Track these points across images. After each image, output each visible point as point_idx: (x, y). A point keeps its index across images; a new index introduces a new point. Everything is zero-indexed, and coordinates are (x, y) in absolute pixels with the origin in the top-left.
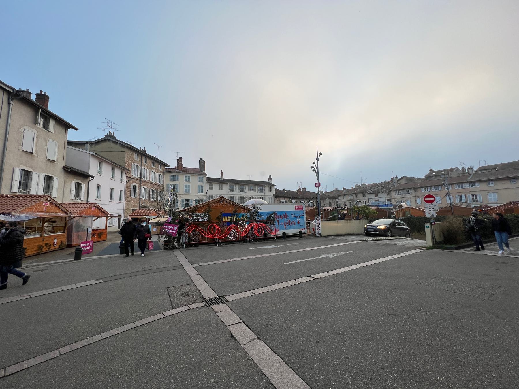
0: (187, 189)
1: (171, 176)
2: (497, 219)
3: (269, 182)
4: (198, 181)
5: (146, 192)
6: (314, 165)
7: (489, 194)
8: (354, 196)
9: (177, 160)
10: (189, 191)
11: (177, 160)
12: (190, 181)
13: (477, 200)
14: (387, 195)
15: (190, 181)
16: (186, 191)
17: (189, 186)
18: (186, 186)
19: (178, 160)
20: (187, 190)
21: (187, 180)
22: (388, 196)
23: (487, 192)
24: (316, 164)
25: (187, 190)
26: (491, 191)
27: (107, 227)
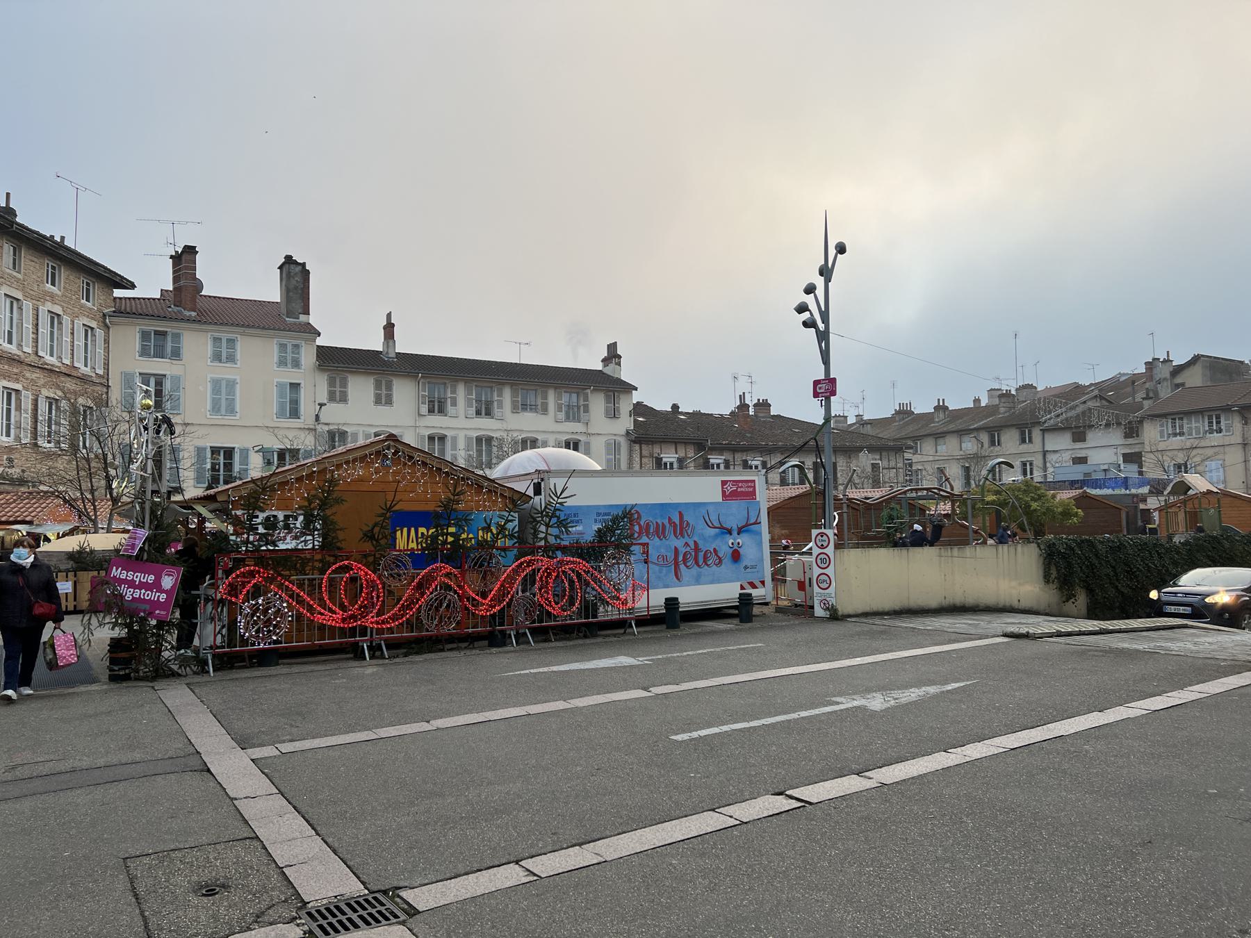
0: (223, 397)
3: (609, 370)
8: (985, 437)
9: (172, 257)
10: (231, 410)
11: (172, 257)
16: (216, 408)
17: (231, 384)
18: (216, 384)
22: (1130, 441)
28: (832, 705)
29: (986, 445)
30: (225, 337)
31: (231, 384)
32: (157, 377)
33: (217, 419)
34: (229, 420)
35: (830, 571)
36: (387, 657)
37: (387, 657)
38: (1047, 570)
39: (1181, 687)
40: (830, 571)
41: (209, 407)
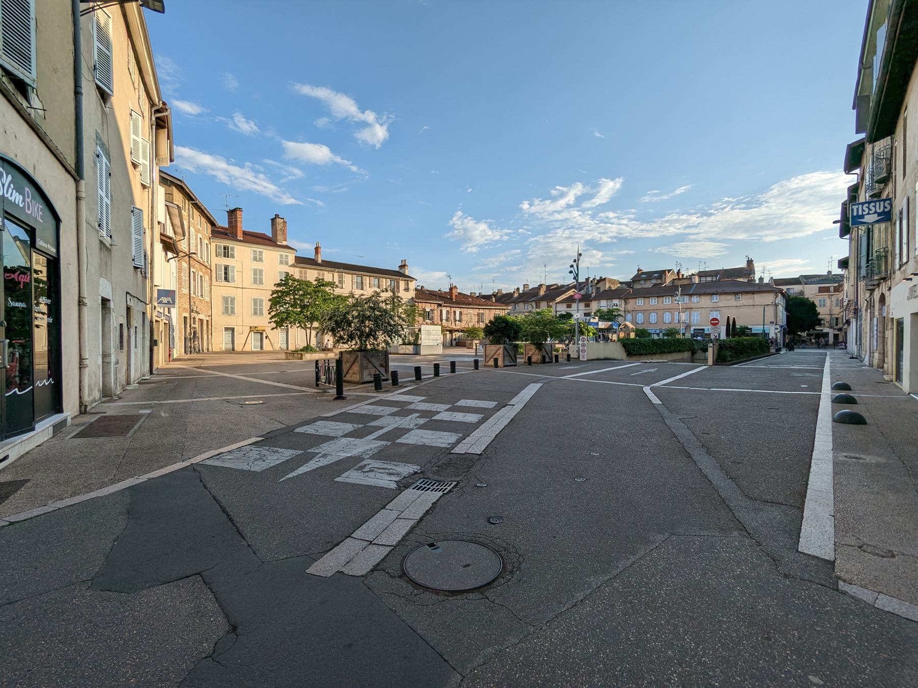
0: (258, 277)
1: (585, 304)
2: (381, 332)
3: (401, 271)
4: (279, 261)
5: (194, 280)
6: (572, 269)
7: (711, 312)
8: (534, 304)
9: (227, 212)
10: (261, 283)
11: (227, 212)
12: (262, 261)
13: (280, 258)
14: (585, 307)
15: (262, 261)
16: (255, 282)
17: (261, 271)
18: (255, 271)
19: (273, 220)
20: (258, 279)
21: (258, 259)
22: (587, 308)
23: (710, 309)
24: (575, 266)
25: (258, 279)
26: (714, 309)
27: (244, 350)
28: (370, 399)
29: (534, 307)
30: (258, 250)
31: (261, 271)
32: (769, 354)
33: (256, 286)
34: (260, 287)
35: (585, 348)
36: (31, 387)
37: (31, 387)
38: (27, 360)
39: (92, 499)
40: (585, 348)
41: (252, 281)
